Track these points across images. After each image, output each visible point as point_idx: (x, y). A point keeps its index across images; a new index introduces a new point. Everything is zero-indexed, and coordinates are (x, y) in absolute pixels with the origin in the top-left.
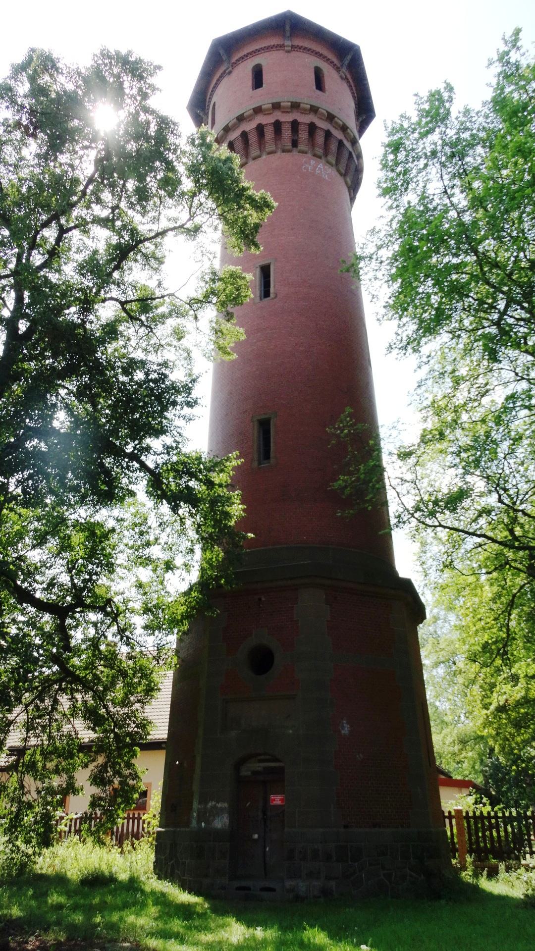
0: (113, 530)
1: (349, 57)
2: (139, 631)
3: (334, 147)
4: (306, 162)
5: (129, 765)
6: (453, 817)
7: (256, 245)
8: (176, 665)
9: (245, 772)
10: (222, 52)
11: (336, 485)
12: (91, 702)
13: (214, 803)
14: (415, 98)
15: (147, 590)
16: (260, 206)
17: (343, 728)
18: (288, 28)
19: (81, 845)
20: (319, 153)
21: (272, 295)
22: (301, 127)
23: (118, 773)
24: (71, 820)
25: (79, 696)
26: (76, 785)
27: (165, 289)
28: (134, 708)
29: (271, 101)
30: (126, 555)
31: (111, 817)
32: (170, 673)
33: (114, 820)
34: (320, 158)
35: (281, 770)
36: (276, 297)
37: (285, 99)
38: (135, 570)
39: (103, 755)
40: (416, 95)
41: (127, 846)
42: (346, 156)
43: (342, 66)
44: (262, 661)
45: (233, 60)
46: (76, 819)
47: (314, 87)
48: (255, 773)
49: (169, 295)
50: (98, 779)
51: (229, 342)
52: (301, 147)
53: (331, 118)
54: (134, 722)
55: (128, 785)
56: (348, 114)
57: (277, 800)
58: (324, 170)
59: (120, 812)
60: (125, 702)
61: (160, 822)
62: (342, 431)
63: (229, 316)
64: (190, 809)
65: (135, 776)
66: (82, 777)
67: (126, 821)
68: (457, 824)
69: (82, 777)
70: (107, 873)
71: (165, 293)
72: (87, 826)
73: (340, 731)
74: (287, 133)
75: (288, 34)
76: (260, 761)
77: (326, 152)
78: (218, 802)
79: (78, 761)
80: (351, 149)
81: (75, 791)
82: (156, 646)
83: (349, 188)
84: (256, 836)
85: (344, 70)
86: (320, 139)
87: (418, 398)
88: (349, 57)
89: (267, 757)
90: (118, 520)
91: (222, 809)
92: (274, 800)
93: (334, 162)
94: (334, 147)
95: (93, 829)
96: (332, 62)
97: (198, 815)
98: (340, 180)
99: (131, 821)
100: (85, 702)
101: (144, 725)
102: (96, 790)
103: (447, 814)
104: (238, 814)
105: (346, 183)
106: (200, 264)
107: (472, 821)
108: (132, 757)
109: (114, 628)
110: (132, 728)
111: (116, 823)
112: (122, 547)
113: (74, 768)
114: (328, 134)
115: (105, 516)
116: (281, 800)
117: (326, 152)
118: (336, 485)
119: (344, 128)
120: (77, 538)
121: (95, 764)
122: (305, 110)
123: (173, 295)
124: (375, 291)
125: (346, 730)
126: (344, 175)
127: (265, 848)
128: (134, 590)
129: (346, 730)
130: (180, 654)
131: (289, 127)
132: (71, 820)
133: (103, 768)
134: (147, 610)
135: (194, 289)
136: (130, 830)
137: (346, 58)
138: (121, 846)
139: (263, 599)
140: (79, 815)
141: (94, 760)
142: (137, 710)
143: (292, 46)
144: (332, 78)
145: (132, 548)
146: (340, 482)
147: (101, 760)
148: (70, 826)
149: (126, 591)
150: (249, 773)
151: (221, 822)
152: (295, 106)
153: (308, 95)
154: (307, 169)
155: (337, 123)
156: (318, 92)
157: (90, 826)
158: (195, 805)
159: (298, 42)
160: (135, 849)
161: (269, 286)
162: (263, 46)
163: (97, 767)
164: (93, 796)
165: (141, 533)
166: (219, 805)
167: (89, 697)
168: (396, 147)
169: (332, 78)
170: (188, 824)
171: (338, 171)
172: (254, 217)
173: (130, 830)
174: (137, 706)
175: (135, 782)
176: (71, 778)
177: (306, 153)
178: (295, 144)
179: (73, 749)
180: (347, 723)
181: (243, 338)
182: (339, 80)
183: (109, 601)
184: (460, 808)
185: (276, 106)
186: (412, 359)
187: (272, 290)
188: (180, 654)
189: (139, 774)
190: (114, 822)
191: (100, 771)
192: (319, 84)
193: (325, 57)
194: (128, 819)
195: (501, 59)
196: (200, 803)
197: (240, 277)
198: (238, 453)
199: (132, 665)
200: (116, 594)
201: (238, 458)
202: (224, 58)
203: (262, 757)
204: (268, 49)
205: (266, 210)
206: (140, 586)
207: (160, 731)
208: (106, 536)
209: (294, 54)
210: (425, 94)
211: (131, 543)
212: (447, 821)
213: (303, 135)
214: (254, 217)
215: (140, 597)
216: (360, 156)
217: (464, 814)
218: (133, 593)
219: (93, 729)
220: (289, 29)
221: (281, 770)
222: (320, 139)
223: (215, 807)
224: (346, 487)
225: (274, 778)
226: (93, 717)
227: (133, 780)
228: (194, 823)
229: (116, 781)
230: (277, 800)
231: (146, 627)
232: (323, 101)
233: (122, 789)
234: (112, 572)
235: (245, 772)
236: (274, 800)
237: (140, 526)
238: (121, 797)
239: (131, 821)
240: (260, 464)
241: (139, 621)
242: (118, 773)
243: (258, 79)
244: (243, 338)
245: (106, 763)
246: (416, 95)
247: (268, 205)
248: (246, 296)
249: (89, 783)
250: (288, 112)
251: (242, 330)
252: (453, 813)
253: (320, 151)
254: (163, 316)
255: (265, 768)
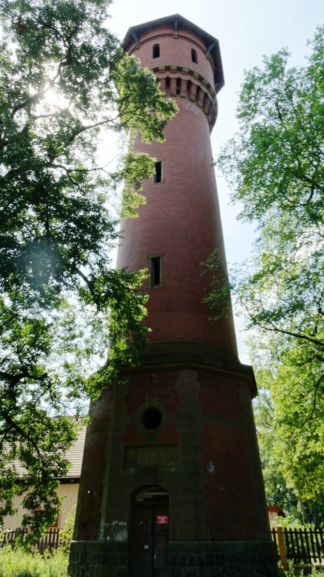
0: (52, 325)
1: (212, 46)
2: (63, 398)
3: (202, 96)
4: (185, 104)
5: (52, 494)
6: (276, 532)
7: (162, 137)
8: (89, 422)
9: (140, 499)
10: (134, 36)
11: (206, 300)
12: (26, 448)
13: (116, 522)
14: (263, 58)
15: (71, 369)
16: (167, 109)
17: (210, 467)
18: (176, 24)
19: (12, 552)
20: (192, 98)
21: (162, 181)
22: (182, 82)
23: (44, 499)
24: (5, 534)
25: (17, 443)
26: (13, 508)
27: (97, 165)
28: (57, 452)
29: (166, 65)
30: (58, 343)
31: (37, 533)
32: (85, 428)
33: (39, 534)
34: (193, 102)
35: (166, 498)
36: (164, 182)
37: (174, 65)
38: (64, 355)
39: (34, 486)
40: (264, 56)
41: (46, 553)
42: (209, 103)
43: (207, 51)
44: (152, 419)
45: (141, 41)
46: (9, 534)
47: (191, 60)
48: (146, 500)
49: (99, 169)
50: (29, 504)
51: (134, 205)
52: (182, 94)
53: (201, 79)
54: (57, 463)
55: (51, 508)
56: (210, 79)
57: (162, 520)
58: (195, 109)
59: (44, 528)
60: (49, 448)
61: (74, 536)
62: (210, 265)
63: (138, 186)
64: (99, 526)
65: (56, 502)
66: (18, 502)
67: (49, 535)
68: (279, 537)
69: (18, 502)
70: (32, 573)
71: (96, 168)
72: (19, 538)
73: (207, 470)
74: (173, 85)
75: (176, 28)
76: (150, 491)
77: (197, 99)
78: (119, 521)
79: (14, 491)
80: (211, 99)
81: (11, 513)
82: (76, 409)
83: (209, 123)
84: (147, 547)
85: (208, 53)
86: (194, 90)
87: (257, 248)
88: (212, 46)
89: (155, 488)
90: (55, 319)
91: (122, 527)
92: (160, 520)
93: (201, 105)
94: (202, 96)
95: (24, 540)
96: (202, 48)
97: (105, 531)
98: (204, 117)
99: (52, 535)
100: (22, 447)
101: (63, 464)
102: (28, 512)
103: (272, 530)
104: (132, 530)
105: (208, 120)
106: (121, 150)
107: (294, 535)
108: (54, 487)
109: (47, 395)
110: (55, 466)
111: (41, 536)
112: (55, 338)
113: (11, 496)
114: (199, 88)
115: (47, 316)
116: (165, 520)
117: (197, 99)
118: (206, 300)
119: (208, 86)
120: (26, 328)
121: (27, 492)
122: (186, 72)
123: (102, 169)
124: (226, 185)
125: (212, 469)
126: (207, 115)
127: (153, 557)
128: (62, 369)
129: (212, 469)
130: (92, 415)
131: (175, 81)
132: (5, 534)
133: (34, 494)
134: (70, 383)
135: (116, 165)
136: (48, 541)
137: (210, 46)
138: (42, 554)
139: (154, 376)
140: (11, 530)
141: (26, 490)
142: (60, 454)
143: (178, 35)
144: (201, 56)
145: (62, 338)
146: (210, 298)
147: (32, 489)
148: (4, 538)
149: (56, 369)
150: (142, 500)
151: (122, 537)
152: (179, 69)
153: (187, 64)
154: (185, 107)
155: (204, 82)
156: (193, 63)
157: (22, 538)
158: (103, 523)
159: (182, 33)
160: (52, 555)
161: (160, 175)
162: (160, 34)
163: (29, 495)
164: (24, 516)
165: (70, 329)
166: (121, 523)
167: (25, 445)
168: (250, 87)
169: (201, 56)
170: (96, 537)
171: (204, 112)
172: (161, 117)
173: (48, 541)
174: (60, 451)
175: (56, 506)
176: (9, 503)
177: (185, 98)
178: (178, 92)
179: (11, 481)
180: (213, 464)
181: (144, 203)
182: (205, 59)
183: (45, 376)
184: (280, 526)
185: (168, 68)
186: (256, 223)
187: (162, 177)
188: (92, 415)
189: (60, 500)
190: (39, 536)
191: (31, 498)
192: (194, 59)
193: (198, 44)
194: (51, 533)
195: (317, 38)
196: (106, 522)
197: (147, 159)
198: (147, 269)
199: (57, 422)
200: (49, 371)
201: (146, 273)
202: (136, 39)
203: (152, 488)
204: (163, 36)
205: (171, 112)
206: (67, 366)
207: (75, 470)
208: (46, 328)
209: (179, 40)
210: (269, 56)
211: (63, 335)
212: (272, 535)
213: (184, 87)
214: (161, 117)
215: (66, 373)
216: (216, 105)
217: (284, 530)
218: (61, 371)
219: (27, 468)
220: (176, 25)
221: (166, 498)
222: (194, 90)
223: (117, 525)
224: (214, 301)
225: (160, 505)
226: (26, 457)
227: (55, 504)
228: (101, 538)
229: (42, 505)
230: (162, 520)
231: (69, 396)
232: (196, 68)
233: (47, 511)
234: (47, 354)
235: (140, 499)
236: (160, 520)
237: (69, 324)
238: (45, 516)
239: (52, 535)
240: (152, 286)
241: (64, 391)
242: (44, 499)
243: (156, 52)
244: (144, 203)
245: (36, 491)
246: (264, 56)
247: (172, 109)
248: (151, 173)
249: (22, 506)
250: (175, 73)
251: (144, 198)
252: (276, 530)
253: (193, 98)
254: (92, 186)
255: (153, 496)
